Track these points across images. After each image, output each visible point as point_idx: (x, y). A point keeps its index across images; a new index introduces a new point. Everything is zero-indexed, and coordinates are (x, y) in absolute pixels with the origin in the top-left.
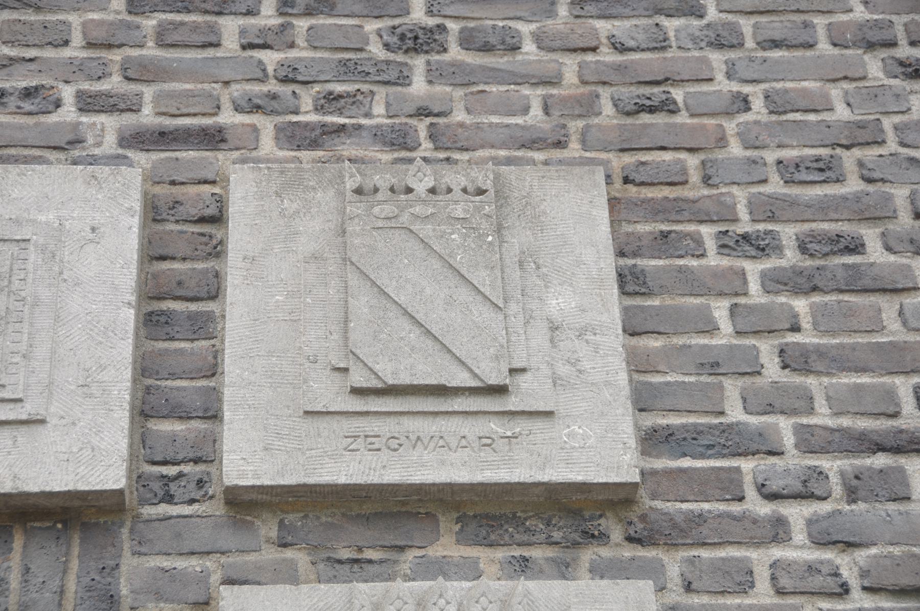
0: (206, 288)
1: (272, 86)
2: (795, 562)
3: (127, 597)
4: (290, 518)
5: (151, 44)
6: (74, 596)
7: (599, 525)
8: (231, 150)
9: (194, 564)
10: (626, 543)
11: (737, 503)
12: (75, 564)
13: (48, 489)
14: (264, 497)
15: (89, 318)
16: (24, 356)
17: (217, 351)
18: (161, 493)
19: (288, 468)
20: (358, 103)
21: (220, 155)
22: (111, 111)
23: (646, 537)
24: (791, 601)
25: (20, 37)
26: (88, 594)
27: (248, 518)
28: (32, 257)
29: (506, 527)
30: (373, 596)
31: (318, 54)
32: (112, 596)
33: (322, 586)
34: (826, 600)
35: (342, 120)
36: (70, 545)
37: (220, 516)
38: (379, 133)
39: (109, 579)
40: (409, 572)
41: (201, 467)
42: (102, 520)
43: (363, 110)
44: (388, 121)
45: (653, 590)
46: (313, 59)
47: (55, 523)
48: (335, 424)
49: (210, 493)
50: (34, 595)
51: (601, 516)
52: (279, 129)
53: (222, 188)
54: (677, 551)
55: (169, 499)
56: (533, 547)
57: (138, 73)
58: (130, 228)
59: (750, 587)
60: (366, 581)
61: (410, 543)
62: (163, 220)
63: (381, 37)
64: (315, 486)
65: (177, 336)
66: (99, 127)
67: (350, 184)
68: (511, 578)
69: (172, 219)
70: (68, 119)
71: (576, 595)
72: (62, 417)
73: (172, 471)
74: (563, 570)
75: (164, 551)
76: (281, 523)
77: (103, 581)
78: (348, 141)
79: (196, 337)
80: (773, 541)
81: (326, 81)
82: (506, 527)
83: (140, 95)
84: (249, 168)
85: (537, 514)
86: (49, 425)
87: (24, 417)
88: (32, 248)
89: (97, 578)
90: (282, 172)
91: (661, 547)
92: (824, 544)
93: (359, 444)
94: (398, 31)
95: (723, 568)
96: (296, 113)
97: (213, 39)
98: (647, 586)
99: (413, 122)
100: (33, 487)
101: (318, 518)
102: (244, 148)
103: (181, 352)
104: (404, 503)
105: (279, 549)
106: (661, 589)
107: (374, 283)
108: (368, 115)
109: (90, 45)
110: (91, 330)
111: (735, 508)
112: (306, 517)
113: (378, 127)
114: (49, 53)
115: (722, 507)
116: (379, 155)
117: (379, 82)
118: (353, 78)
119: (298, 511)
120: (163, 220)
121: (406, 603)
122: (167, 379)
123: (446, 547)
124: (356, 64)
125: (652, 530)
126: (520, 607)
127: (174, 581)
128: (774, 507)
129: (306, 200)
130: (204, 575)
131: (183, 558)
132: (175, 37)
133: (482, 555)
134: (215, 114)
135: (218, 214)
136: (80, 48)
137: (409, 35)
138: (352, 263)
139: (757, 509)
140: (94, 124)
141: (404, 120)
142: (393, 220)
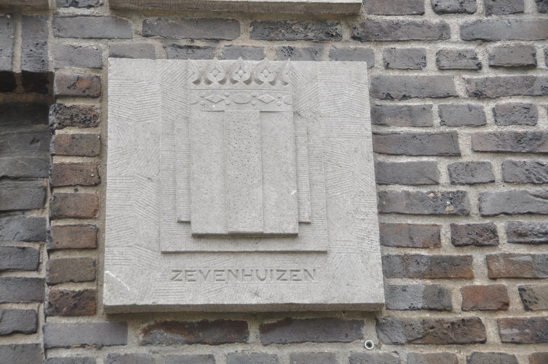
2: (451, 51)
3: (52, 62)
4: (150, 19)
7: (336, 29)
9: (92, 44)
10: (351, 40)
11: (420, 16)
12: (19, 40)
14: (134, 6)
23: (363, 36)
24: (447, 74)
26: (29, 59)
27: (124, 18)
29: (280, 29)
30: (200, 68)
32: (43, 61)
33: (169, 61)
34: (468, 73)
36: (16, 29)
37: (107, 17)
39: (41, 51)
40: (221, 54)
42: (35, 15)
45: (366, 67)
47: (6, 14)
51: (337, 24)
54: (382, 45)
56: (296, 42)
59: (423, 66)
60: (196, 59)
61: (222, 38)
68: (283, 60)
71: (321, 70)
74: (314, 55)
75: (74, 36)
76: (144, 22)
77: (37, 51)
80: (439, 39)
82: (280, 29)
85: (299, 22)
89: (34, 49)
91: (372, 43)
92: (470, 41)
95: (408, 55)
98: (363, 65)
101: (167, 20)
104: (219, 13)
105: (144, 38)
106: (371, 67)
111: (419, 19)
112: (159, 19)
115: (410, 19)
119: (155, 16)
121: (220, 72)
123: (244, 40)
125: (368, 32)
126: (287, 76)
128: (442, 19)
130: (99, 52)
133: (265, 46)
139: (432, 20)
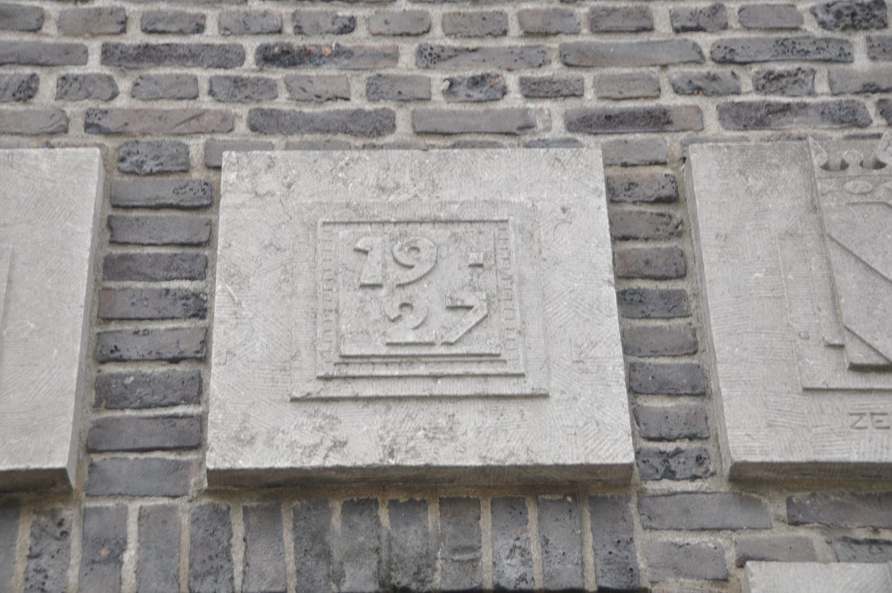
0: (674, 268)
1: (710, 68)
3: (646, 571)
4: (797, 496)
5: (585, 31)
6: (593, 568)
8: (677, 131)
9: (705, 540)
13: (561, 462)
14: (771, 474)
15: (573, 296)
16: (520, 332)
17: (695, 330)
18: (662, 469)
19: (796, 445)
20: (800, 82)
21: (668, 137)
22: (555, 97)
25: (462, 29)
26: (608, 567)
27: (755, 495)
28: (513, 237)
31: (753, 35)
32: (631, 570)
35: (785, 100)
37: (726, 493)
38: (827, 111)
39: (626, 553)
41: (696, 445)
43: (805, 89)
44: (834, 99)
46: (749, 40)
48: (837, 401)
49: (712, 469)
50: (557, 566)
52: (722, 112)
53: (673, 169)
55: (670, 474)
57: (576, 59)
58: (599, 208)
62: (621, 201)
63: (816, 15)
64: (826, 463)
65: (653, 314)
66: (546, 112)
67: (817, 161)
69: (629, 200)
70: (516, 106)
72: (563, 392)
73: (669, 447)
75: (674, 526)
76: (789, 501)
77: (620, 554)
78: (795, 120)
79: (671, 315)
81: (765, 61)
83: (581, 81)
84: (708, 147)
86: (552, 400)
87: (528, 391)
88: (511, 229)
89: (614, 551)
90: (742, 151)
93: (866, 421)
94: (834, 8)
96: (738, 93)
97: (645, 23)
99: (860, 99)
100: (547, 460)
101: (826, 497)
102: (691, 129)
103: (660, 330)
105: (791, 527)
107: (858, 259)
108: (811, 93)
109: (528, 34)
110: (577, 307)
112: (813, 495)
113: (825, 105)
114: (490, 43)
116: (829, 133)
117: (819, 60)
118: (792, 57)
119: (804, 489)
120: (621, 201)
122: (650, 357)
124: (794, 43)
127: (690, 556)
129: (771, 178)
131: (694, 533)
132: (610, 23)
134: (657, 97)
135: (674, 195)
136: (521, 37)
137: (846, 12)
138: (832, 239)
140: (541, 110)
141: (850, 97)
142: (869, 196)
